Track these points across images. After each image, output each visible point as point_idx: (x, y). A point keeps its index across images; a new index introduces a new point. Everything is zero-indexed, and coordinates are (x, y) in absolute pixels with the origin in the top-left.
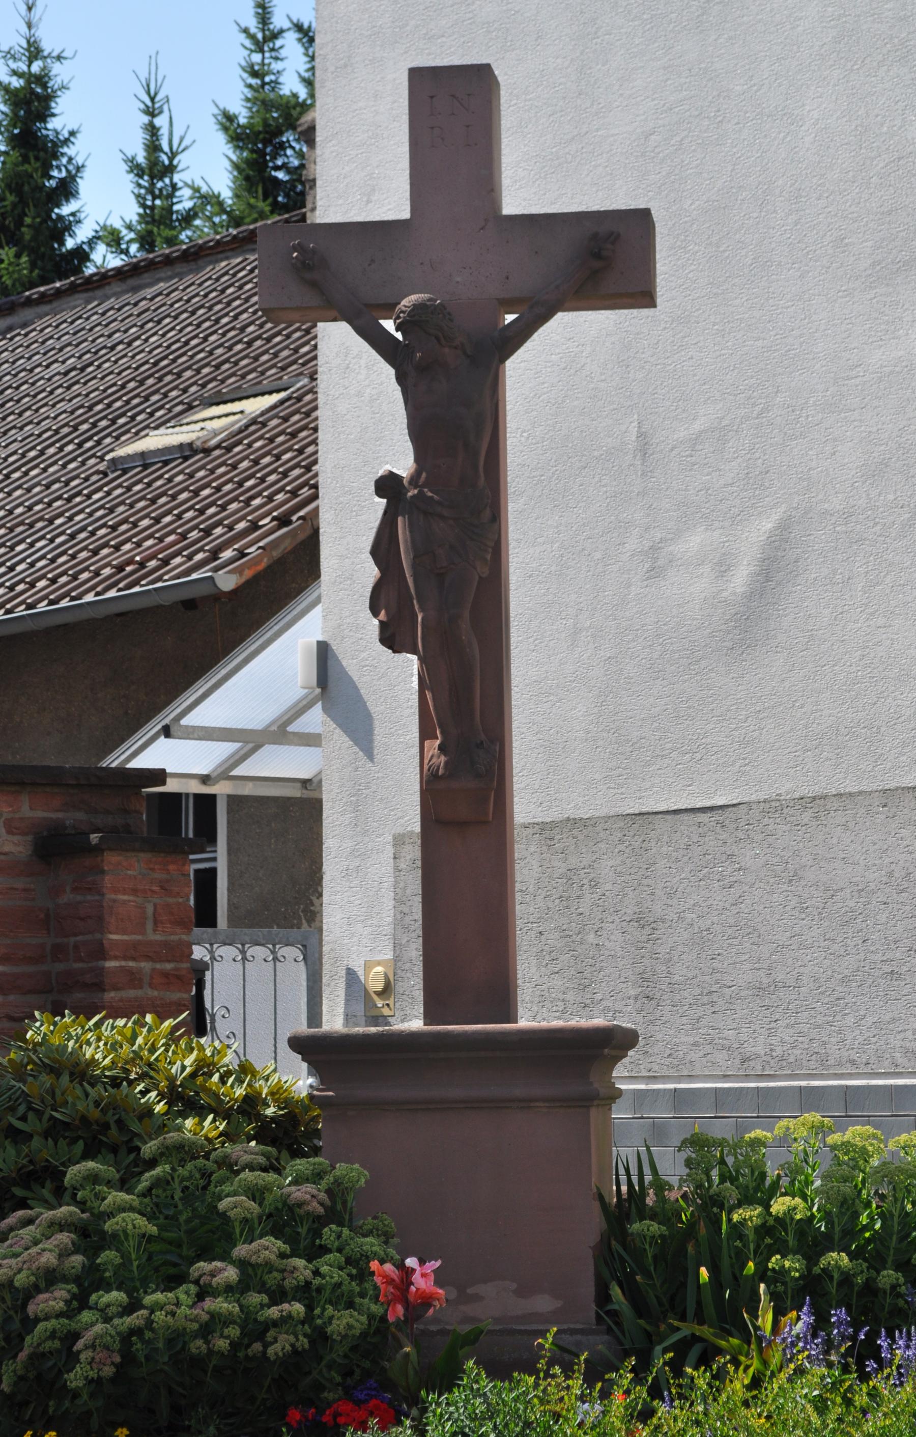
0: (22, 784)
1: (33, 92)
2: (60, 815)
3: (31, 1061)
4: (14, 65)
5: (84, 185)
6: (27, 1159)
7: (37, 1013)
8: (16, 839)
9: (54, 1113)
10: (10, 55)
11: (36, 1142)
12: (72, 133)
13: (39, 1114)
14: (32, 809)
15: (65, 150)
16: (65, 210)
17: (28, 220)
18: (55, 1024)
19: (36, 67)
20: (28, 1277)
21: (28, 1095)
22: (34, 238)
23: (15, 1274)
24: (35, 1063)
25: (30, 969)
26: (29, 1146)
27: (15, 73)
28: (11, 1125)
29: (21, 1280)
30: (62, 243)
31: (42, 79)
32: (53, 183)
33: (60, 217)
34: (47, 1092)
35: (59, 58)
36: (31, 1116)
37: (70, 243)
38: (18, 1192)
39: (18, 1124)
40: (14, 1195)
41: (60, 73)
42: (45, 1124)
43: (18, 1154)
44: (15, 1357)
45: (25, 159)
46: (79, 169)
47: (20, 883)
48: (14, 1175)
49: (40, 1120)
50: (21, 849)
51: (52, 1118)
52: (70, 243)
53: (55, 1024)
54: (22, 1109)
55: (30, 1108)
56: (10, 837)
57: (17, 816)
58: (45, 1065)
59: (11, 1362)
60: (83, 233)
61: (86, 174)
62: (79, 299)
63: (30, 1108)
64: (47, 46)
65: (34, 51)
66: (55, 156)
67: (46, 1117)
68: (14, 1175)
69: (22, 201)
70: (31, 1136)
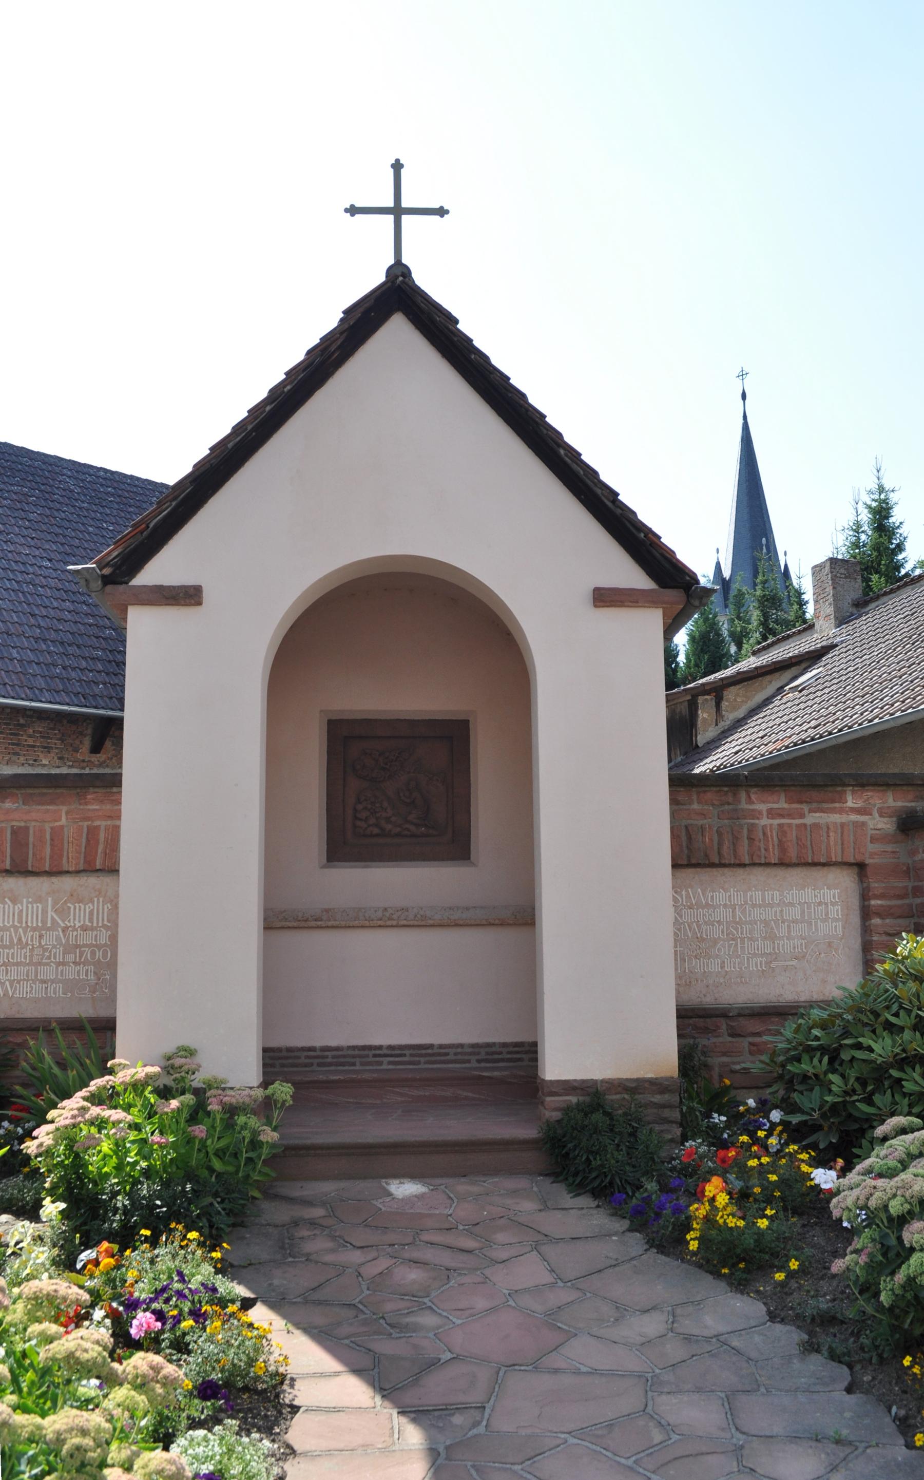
0: (888, 785)
1: (882, 507)
2: (913, 804)
3: (900, 971)
4: (873, 497)
5: (908, 545)
6: (900, 1048)
7: (904, 934)
8: (885, 820)
9: (920, 1013)
10: (870, 492)
11: (907, 1035)
12: (901, 523)
13: (909, 1012)
14: (894, 801)
15: (898, 531)
16: (900, 557)
17: (883, 562)
18: (917, 942)
19: (882, 497)
20: (902, 1205)
21: (900, 998)
22: (886, 570)
23: (890, 1199)
24: (904, 973)
25: (899, 902)
26: (901, 1038)
27: (873, 500)
28: (887, 1019)
29: (896, 1207)
30: (899, 572)
31: (885, 501)
32: (893, 546)
33: (898, 561)
34: (914, 995)
35: (893, 491)
36: (902, 1013)
37: (903, 572)
38: (895, 1073)
39: (893, 1020)
40: (891, 1076)
41: (893, 498)
42: (913, 1021)
43: (894, 1041)
44: (893, 1273)
45: (880, 536)
46: (905, 539)
47: (889, 848)
48: (891, 1060)
49: (909, 1016)
50: (888, 826)
51: (918, 1016)
52: (903, 572)
53: (917, 942)
54: (895, 1007)
55: (901, 1007)
56: (882, 819)
57: (886, 805)
58: (911, 974)
59: (888, 1279)
60: (908, 567)
61: (908, 540)
62: (909, 588)
63: (901, 1007)
64: (887, 486)
65: (881, 489)
66: (894, 534)
67: (913, 1015)
68: (891, 1060)
69: (880, 554)
70: (902, 1029)
